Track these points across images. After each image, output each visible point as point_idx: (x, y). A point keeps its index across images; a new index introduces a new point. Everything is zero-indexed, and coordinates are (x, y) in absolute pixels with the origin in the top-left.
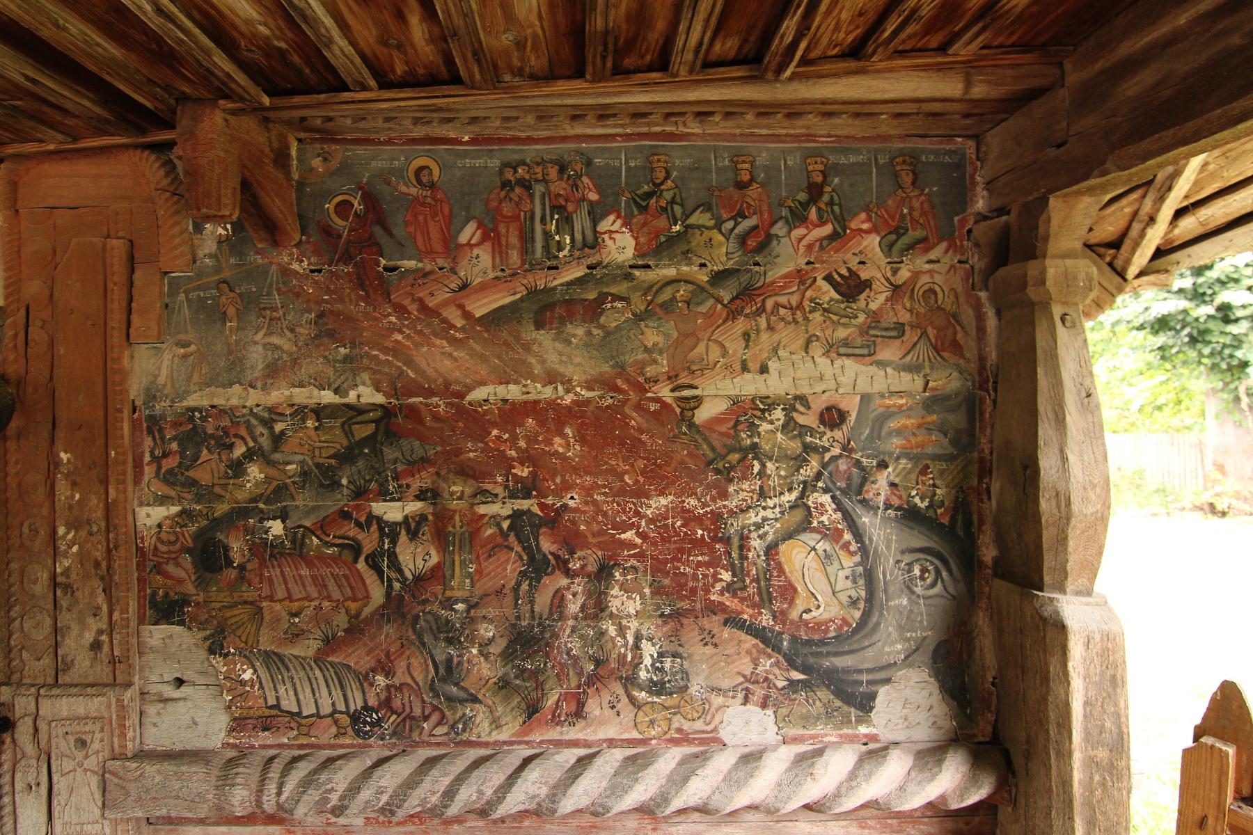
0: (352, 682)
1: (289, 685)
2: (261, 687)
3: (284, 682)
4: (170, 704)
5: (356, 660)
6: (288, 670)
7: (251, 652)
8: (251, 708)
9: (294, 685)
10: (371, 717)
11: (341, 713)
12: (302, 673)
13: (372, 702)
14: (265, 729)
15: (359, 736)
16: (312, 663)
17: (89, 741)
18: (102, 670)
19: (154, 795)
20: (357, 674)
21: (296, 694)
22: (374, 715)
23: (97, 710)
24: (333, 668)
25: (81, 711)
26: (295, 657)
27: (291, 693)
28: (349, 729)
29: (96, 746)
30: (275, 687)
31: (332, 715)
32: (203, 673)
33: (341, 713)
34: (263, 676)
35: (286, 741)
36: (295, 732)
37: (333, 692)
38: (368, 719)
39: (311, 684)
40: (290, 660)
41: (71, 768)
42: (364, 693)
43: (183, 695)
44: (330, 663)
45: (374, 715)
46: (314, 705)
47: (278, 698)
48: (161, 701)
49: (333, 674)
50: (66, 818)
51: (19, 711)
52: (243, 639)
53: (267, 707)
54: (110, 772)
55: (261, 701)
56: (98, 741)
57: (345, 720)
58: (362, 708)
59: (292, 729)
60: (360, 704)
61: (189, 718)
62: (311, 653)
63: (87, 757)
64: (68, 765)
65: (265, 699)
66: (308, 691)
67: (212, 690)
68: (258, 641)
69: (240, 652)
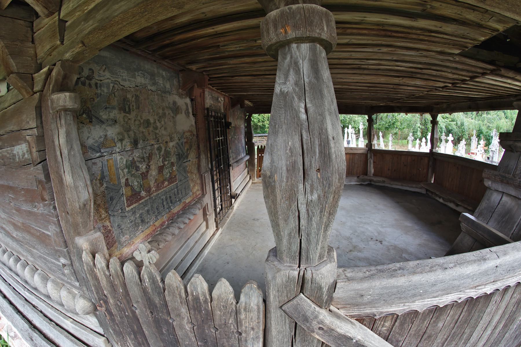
14: (502, 182)
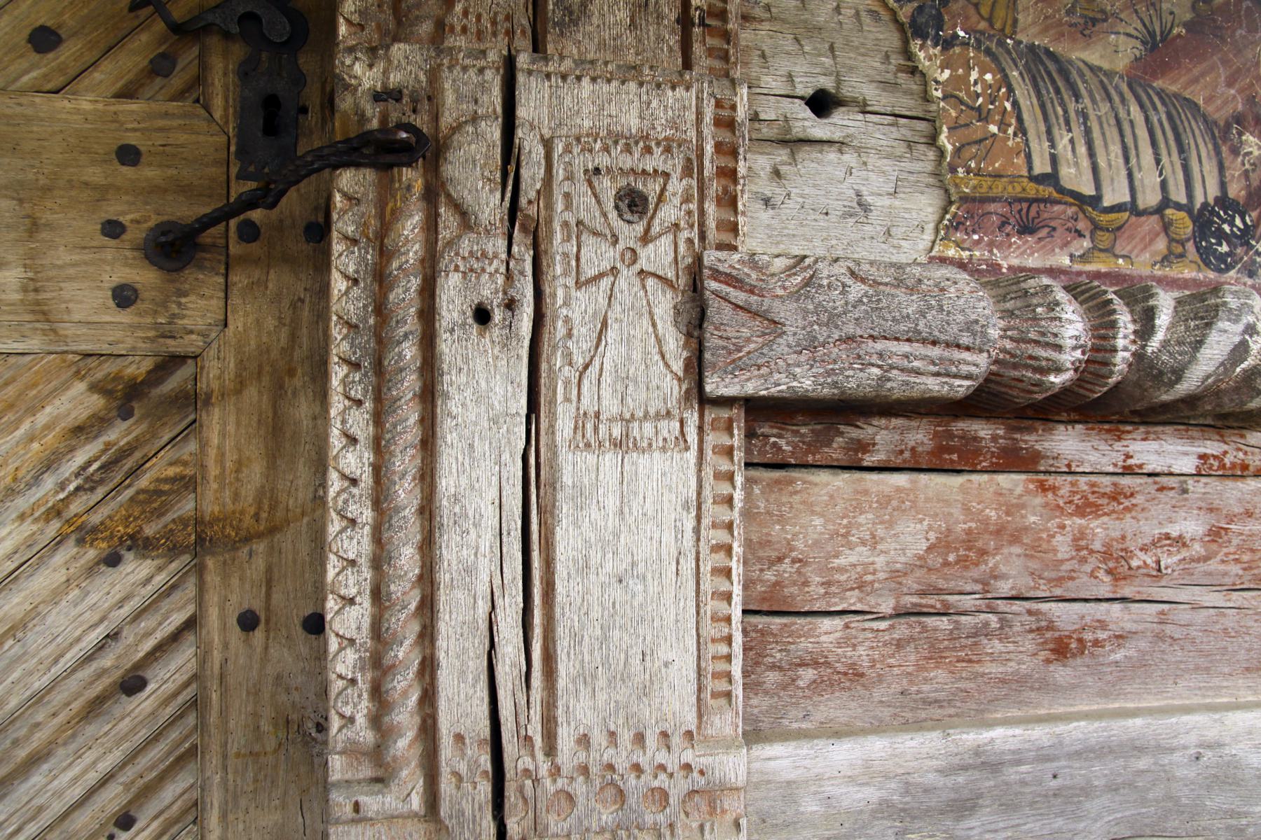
0: (1200, 141)
1: (1078, 131)
2: (1022, 130)
3: (1067, 123)
4: (804, 153)
5: (1207, 93)
6: (1077, 96)
7: (1002, 44)
8: (997, 176)
9: (1088, 132)
10: (1232, 224)
11: (1178, 207)
12: (1105, 108)
13: (1236, 190)
14: (1026, 229)
15: (1207, 264)
16: (1125, 88)
17: (652, 200)
18: (660, 39)
19: (850, 329)
20: (1209, 124)
21: (1092, 154)
22: (1238, 222)
23: (673, 124)
24: (1164, 103)
25: (631, 122)
26: (1093, 69)
27: (1082, 150)
28: (1190, 246)
29: (669, 213)
30: (1049, 132)
31: (1159, 210)
32: (886, 85)
33: (1178, 207)
34: (1024, 103)
35: (1066, 261)
36: (1086, 244)
37: (1165, 160)
38: (1226, 227)
39: (1122, 135)
40: (1082, 75)
41: (606, 265)
42: (1221, 168)
43: (837, 136)
44: (1160, 94)
45: (1238, 222)
46: (1125, 183)
47: (1054, 160)
48: (783, 142)
49: (1164, 117)
50: (585, 401)
51: (452, 108)
52: (985, 11)
53: (1032, 178)
54: (717, 275)
55: (1020, 161)
56: (677, 201)
57: (1185, 225)
58: (1217, 199)
59: (1080, 235)
60: (1213, 191)
61: (851, 193)
62: (1122, 63)
63: (646, 239)
64: (597, 256)
65: (1029, 157)
66: (1116, 149)
67: (906, 129)
68: (1015, 21)
69: (978, 41)
